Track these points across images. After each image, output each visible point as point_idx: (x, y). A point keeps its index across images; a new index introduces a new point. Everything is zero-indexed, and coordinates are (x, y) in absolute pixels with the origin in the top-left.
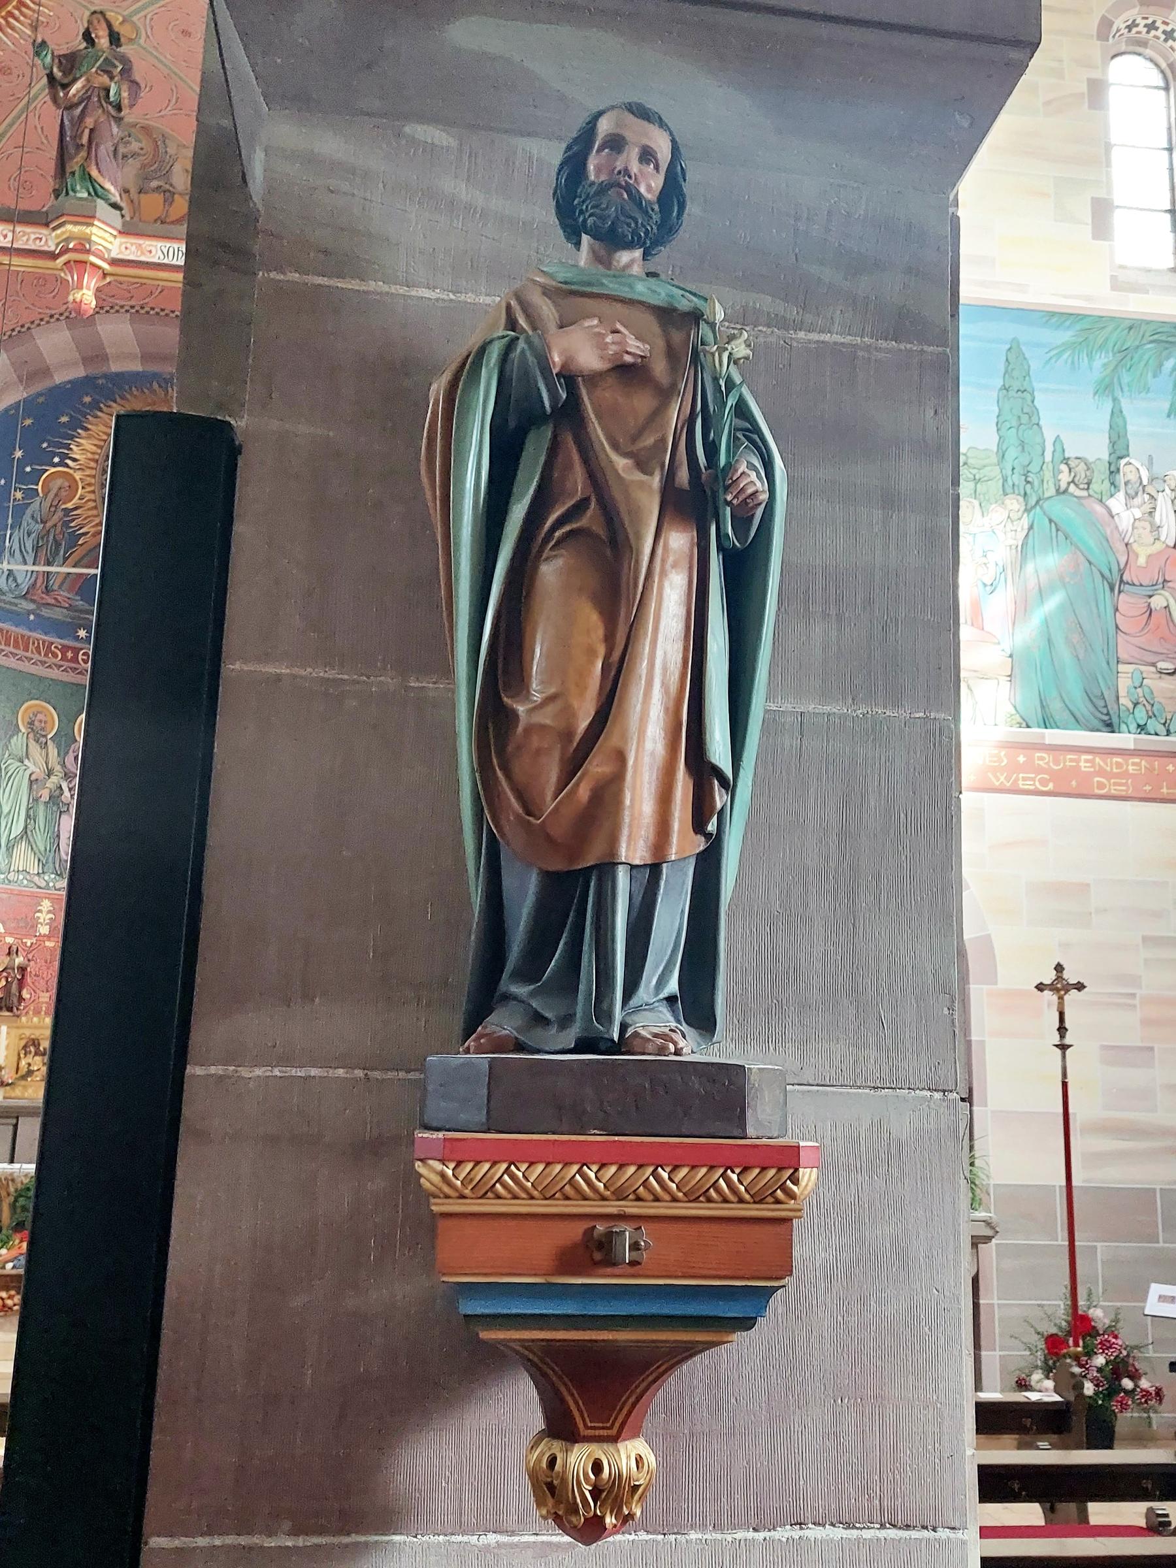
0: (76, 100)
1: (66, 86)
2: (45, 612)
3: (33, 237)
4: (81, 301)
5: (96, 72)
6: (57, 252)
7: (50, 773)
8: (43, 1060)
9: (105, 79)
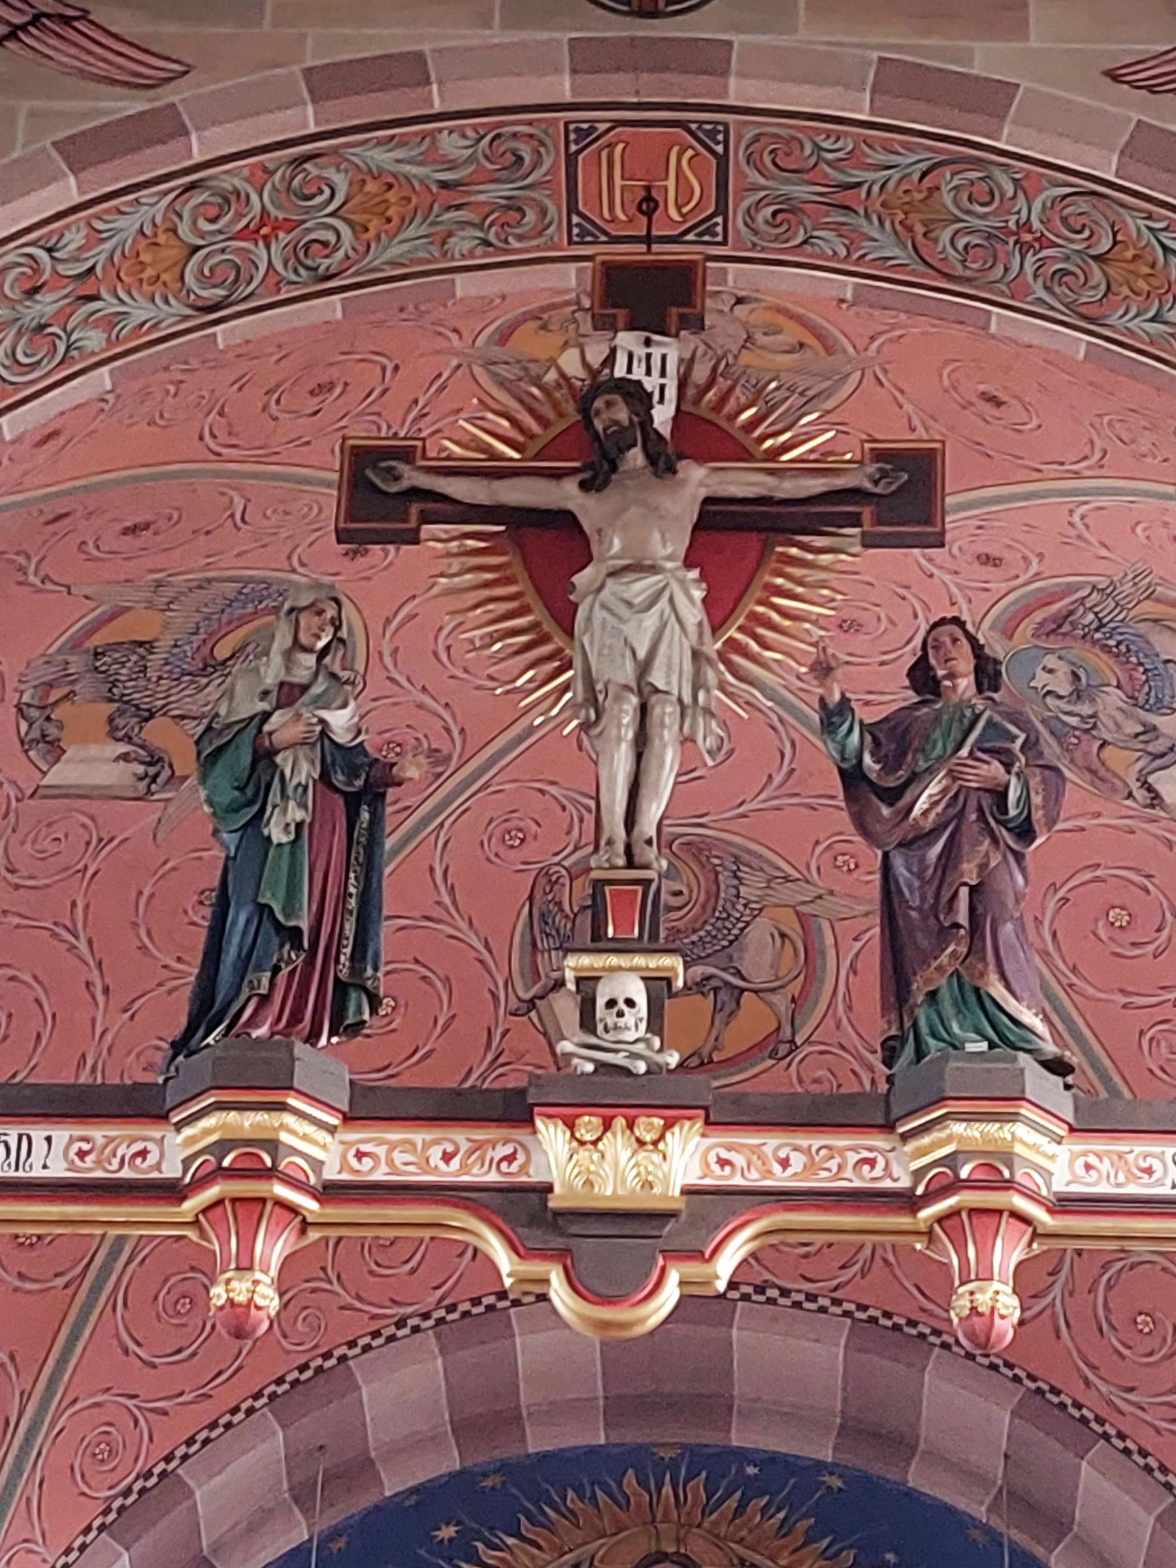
0: (929, 823)
1: (891, 796)
3: (853, 1157)
4: (993, 1309)
5: (971, 753)
6: (920, 1191)
9: (995, 768)
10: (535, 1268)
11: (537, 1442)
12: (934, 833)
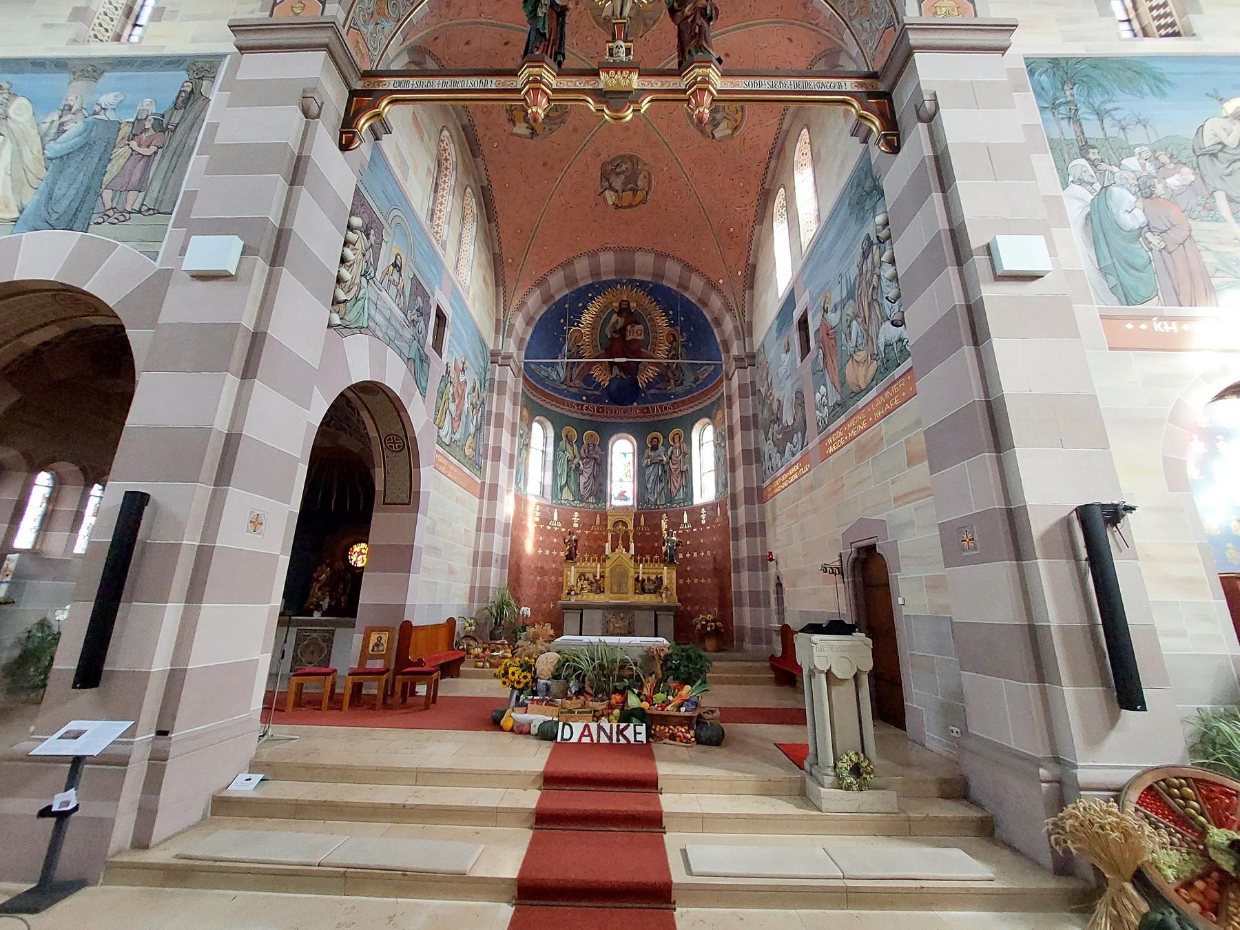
2: (571, 390)
7: (575, 457)
10: (600, 106)
11: (604, 279)
12: (690, 16)
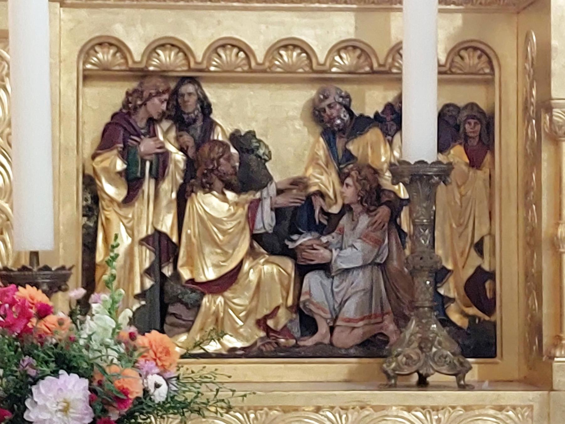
8: (251, 219)
